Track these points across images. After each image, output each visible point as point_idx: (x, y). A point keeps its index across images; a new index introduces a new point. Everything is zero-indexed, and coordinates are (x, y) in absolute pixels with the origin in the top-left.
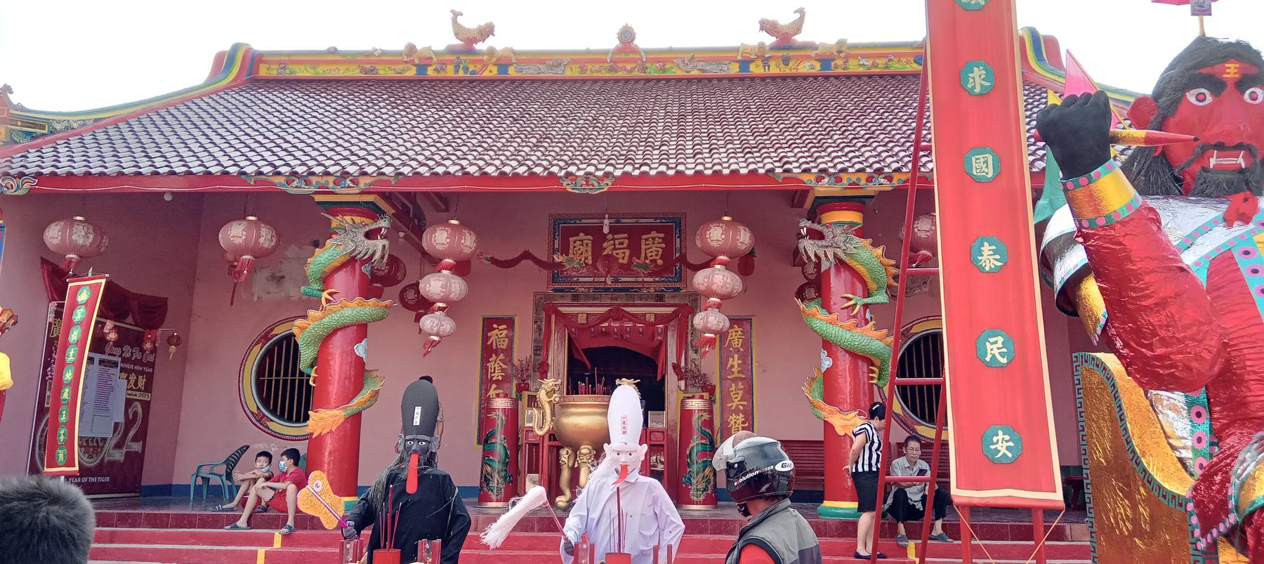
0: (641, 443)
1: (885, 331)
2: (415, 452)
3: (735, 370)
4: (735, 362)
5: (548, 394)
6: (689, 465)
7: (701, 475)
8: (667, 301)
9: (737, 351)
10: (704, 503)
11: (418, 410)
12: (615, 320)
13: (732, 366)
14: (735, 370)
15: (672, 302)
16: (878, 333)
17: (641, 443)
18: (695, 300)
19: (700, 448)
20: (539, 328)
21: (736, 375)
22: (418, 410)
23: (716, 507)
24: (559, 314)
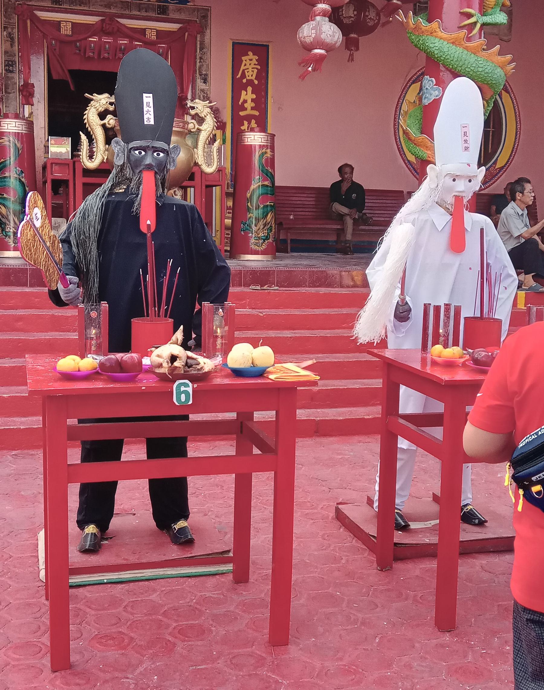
0: (480, 165)
1: (509, 57)
2: (149, 167)
3: (249, 105)
4: (248, 96)
5: (102, 115)
6: (249, 210)
7: (261, 223)
8: (172, 16)
9: (250, 83)
10: (263, 253)
11: (148, 99)
12: (108, 34)
13: (245, 101)
14: (249, 105)
15: (177, 16)
16: (501, 59)
17: (480, 165)
18: (205, 17)
19: (261, 191)
20: (10, 35)
21: (249, 112)
22: (148, 99)
23: (275, 258)
24: (35, 20)
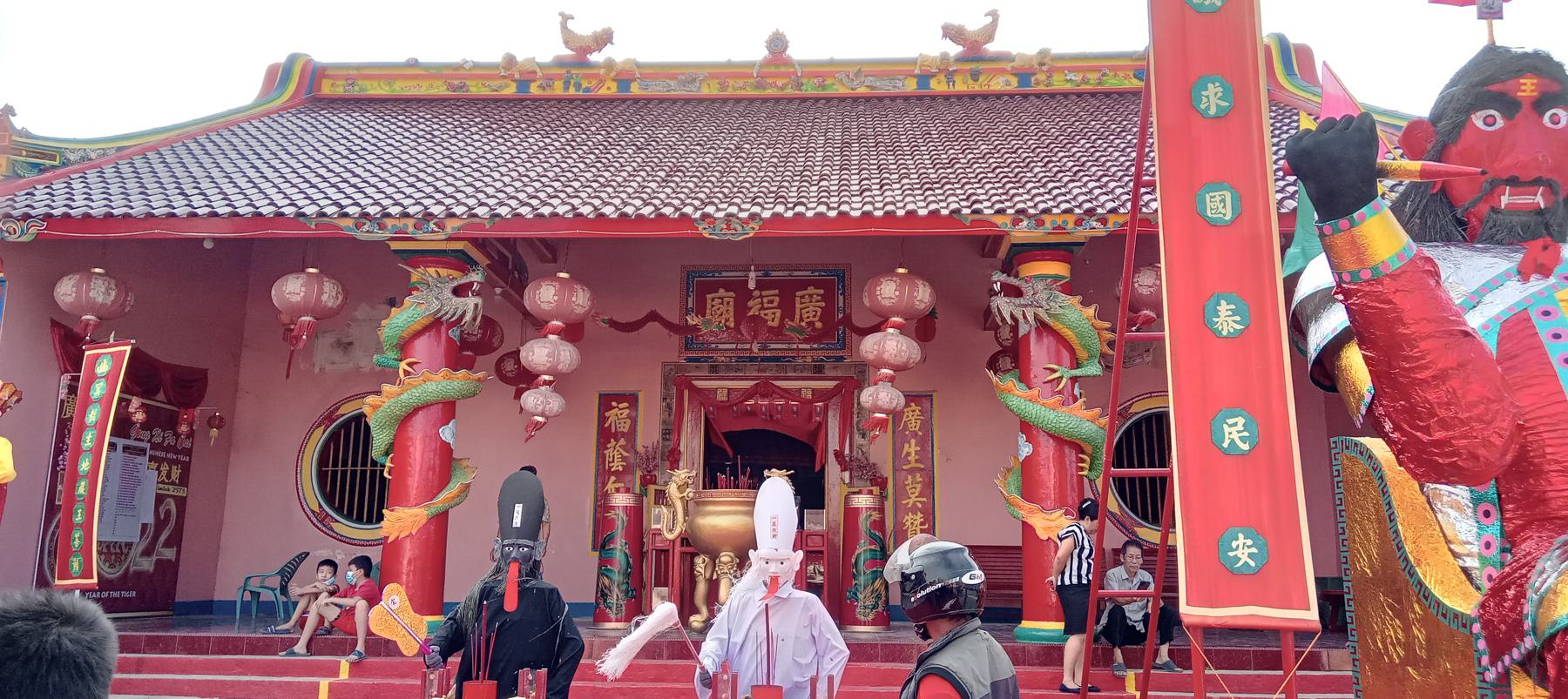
1: (1098, 410)
2: (515, 560)
3: (912, 458)
4: (912, 448)
5: (680, 488)
6: (854, 576)
7: (870, 589)
8: (828, 373)
9: (915, 435)
10: (873, 623)
11: (519, 508)
12: (763, 396)
13: (908, 454)
14: (912, 458)
15: (834, 374)
16: (1090, 413)
18: (862, 372)
19: (868, 555)
20: (669, 407)
21: (913, 465)
22: (519, 508)
23: (889, 628)
24: (693, 389)
